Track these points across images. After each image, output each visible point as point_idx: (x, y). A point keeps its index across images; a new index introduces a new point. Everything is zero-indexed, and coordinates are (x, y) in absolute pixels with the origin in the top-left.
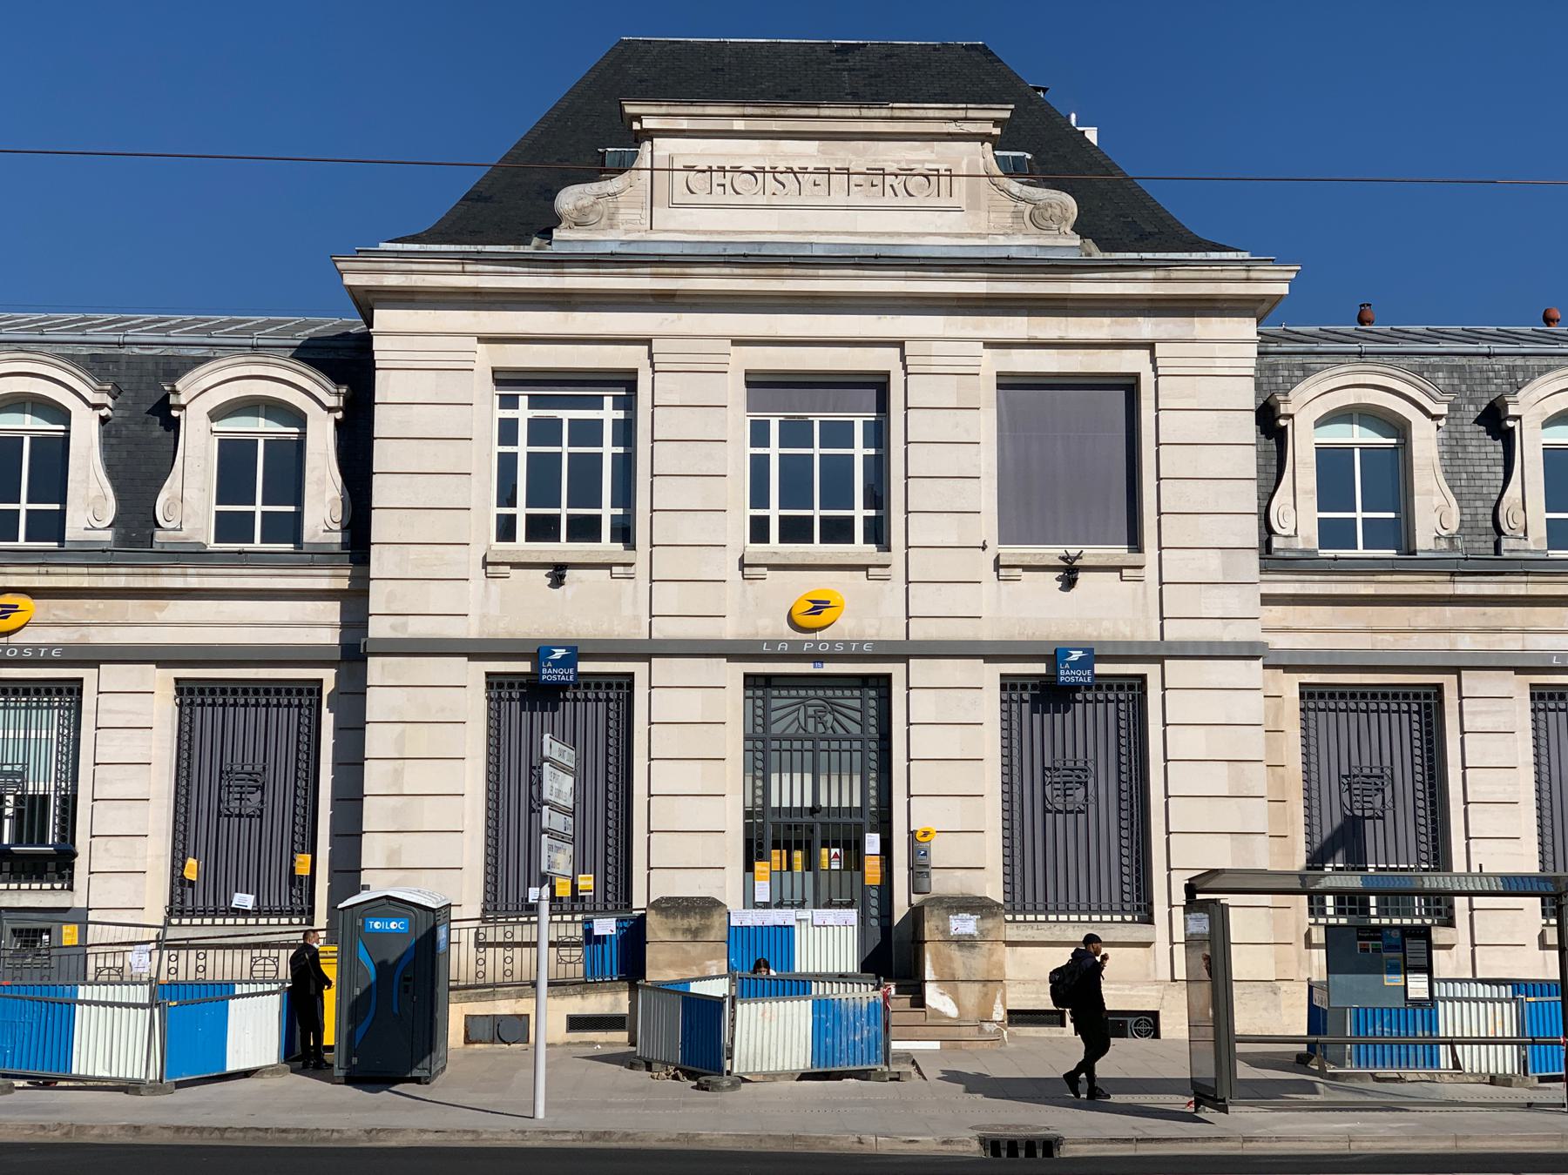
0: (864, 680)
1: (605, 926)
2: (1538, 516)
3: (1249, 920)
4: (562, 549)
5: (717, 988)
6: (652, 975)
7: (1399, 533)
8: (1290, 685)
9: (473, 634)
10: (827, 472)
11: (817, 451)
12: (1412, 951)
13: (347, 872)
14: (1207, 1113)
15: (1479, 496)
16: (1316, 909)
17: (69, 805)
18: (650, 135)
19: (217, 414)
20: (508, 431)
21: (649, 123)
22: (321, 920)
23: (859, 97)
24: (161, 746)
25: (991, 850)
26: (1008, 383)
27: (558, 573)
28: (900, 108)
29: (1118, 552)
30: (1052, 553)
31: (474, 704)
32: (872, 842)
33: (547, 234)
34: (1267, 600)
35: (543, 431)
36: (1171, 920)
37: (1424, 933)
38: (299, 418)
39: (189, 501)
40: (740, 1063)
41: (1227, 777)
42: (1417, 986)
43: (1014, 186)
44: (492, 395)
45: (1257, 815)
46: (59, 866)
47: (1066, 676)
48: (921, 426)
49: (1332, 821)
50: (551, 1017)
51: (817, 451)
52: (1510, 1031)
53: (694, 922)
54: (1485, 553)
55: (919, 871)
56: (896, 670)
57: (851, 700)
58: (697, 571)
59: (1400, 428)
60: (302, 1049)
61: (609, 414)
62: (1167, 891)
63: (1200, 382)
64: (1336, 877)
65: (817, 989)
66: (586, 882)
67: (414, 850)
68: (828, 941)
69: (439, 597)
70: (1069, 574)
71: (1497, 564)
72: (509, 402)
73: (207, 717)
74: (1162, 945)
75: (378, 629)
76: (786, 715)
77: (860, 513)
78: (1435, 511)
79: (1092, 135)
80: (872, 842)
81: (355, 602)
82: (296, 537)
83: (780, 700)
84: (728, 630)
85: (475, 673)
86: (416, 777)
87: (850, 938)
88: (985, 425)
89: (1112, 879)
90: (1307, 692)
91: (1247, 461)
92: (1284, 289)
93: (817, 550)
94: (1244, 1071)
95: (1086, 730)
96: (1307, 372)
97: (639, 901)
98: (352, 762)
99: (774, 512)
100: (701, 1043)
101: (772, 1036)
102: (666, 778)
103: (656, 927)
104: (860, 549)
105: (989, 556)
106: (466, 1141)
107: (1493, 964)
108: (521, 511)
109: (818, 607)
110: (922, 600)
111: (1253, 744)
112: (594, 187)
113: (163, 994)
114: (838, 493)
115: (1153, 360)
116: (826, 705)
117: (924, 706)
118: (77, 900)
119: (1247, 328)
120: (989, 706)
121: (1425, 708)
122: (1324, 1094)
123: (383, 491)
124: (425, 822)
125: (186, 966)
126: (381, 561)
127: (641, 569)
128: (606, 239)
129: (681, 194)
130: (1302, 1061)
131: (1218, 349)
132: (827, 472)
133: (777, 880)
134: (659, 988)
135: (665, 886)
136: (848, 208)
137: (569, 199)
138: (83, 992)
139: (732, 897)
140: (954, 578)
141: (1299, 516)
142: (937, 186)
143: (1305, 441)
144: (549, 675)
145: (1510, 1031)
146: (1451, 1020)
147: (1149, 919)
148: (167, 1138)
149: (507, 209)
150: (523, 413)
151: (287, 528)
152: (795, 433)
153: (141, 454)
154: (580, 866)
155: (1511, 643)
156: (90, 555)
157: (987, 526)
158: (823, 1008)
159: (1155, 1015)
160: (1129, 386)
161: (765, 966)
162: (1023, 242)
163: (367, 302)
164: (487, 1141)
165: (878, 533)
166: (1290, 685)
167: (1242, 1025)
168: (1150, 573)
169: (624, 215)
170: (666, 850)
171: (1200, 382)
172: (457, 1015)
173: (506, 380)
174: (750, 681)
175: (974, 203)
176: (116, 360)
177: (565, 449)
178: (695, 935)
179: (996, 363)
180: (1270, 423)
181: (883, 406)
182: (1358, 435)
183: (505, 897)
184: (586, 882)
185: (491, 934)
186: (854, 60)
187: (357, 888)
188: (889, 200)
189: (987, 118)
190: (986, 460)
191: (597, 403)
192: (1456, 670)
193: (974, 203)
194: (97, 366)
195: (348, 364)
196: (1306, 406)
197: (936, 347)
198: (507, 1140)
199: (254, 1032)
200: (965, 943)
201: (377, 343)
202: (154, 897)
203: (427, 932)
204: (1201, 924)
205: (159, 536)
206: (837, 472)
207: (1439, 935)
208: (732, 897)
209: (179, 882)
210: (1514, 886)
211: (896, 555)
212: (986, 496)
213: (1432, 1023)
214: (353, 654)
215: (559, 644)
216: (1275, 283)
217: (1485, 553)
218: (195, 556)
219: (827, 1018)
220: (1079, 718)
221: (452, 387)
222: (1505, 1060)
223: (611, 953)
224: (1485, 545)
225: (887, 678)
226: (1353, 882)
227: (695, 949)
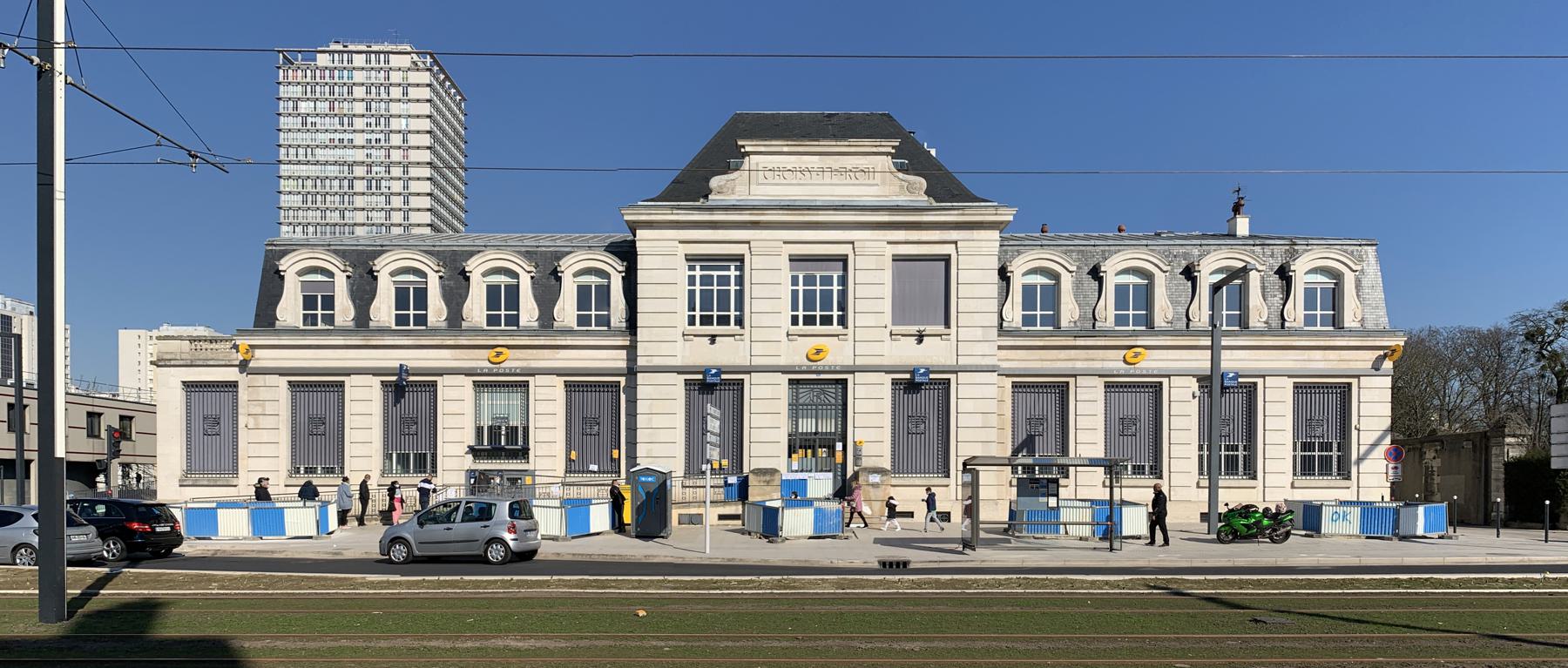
0: (837, 381)
1: (733, 480)
2: (1111, 313)
3: (986, 476)
4: (715, 329)
5: (777, 504)
6: (751, 499)
7: (1054, 321)
8: (1008, 382)
10: (822, 298)
11: (818, 288)
12: (1051, 487)
13: (632, 458)
14: (968, 551)
15: (1178, 303)
16: (1014, 471)
17: (526, 430)
18: (748, 154)
19: (576, 275)
20: (692, 280)
22: (623, 475)
23: (835, 137)
24: (560, 407)
26: (897, 259)
27: (713, 338)
28: (853, 141)
29: (941, 329)
30: (914, 329)
31: (680, 391)
32: (839, 446)
33: (706, 197)
34: (1000, 348)
35: (706, 280)
36: (956, 475)
37: (1056, 481)
39: (566, 310)
40: (784, 533)
41: (982, 420)
42: (1052, 502)
43: (900, 175)
44: (686, 265)
45: (992, 435)
46: (523, 453)
47: (918, 379)
48: (861, 277)
49: (1022, 436)
50: (711, 515)
51: (818, 288)
52: (1089, 519)
53: (768, 478)
54: (1090, 328)
55: (857, 457)
56: (849, 377)
57: (831, 389)
58: (769, 337)
59: (1056, 276)
60: (618, 526)
61: (733, 273)
62: (955, 465)
63: (976, 256)
64: (1022, 459)
65: (816, 504)
66: (725, 462)
67: (657, 450)
68: (821, 485)
69: (665, 349)
70: (920, 338)
71: (1094, 332)
72: (692, 268)
73: (576, 396)
74: (953, 486)
75: (641, 362)
76: (806, 395)
77: (835, 313)
78: (1070, 311)
79: (933, 152)
80: (839, 446)
81: (632, 350)
82: (608, 325)
83: (802, 389)
84: (782, 361)
85: (887, 379)
86: (657, 421)
87: (830, 483)
88: (887, 277)
89: (934, 463)
90: (1015, 385)
91: (993, 290)
92: (1011, 218)
93: (818, 328)
94: (982, 535)
95: (927, 399)
96: (1019, 253)
97: (746, 470)
98: (632, 415)
99: (801, 313)
100: (770, 526)
101: (797, 522)
103: (752, 480)
104: (835, 328)
106: (680, 561)
107: (1084, 493)
108: (698, 313)
109: (818, 351)
110: (963, 348)
111: (992, 406)
113: (565, 503)
114: (827, 305)
116: (821, 391)
118: (530, 467)
119: (995, 234)
121: (1061, 391)
122: (1014, 543)
123: (642, 305)
124: (661, 435)
125: (573, 493)
126: (642, 334)
127: (747, 337)
128: (731, 199)
130: (1006, 531)
132: (822, 298)
133: (801, 461)
134: (753, 504)
137: (715, 182)
138: (535, 502)
139: (783, 468)
140: (873, 340)
141: (1014, 314)
142: (867, 175)
143: (1018, 282)
144: (710, 380)
145: (1089, 519)
146: (1065, 515)
148: (570, 558)
149: (690, 187)
150: (698, 273)
151: (605, 321)
152: (809, 280)
153: (548, 290)
154: (722, 456)
155: (1097, 365)
156: (529, 332)
157: (887, 318)
158: (817, 511)
160: (946, 259)
161: (796, 495)
162: (903, 199)
163: (633, 227)
164: (687, 561)
165: (843, 321)
166: (1008, 382)
168: (953, 337)
171: (976, 256)
172: (675, 513)
173: (690, 259)
174: (791, 381)
175: (884, 183)
176: (536, 253)
177: (715, 288)
180: (1004, 274)
181: (845, 269)
182: (1039, 280)
183: (694, 466)
184: (725, 462)
185: (687, 483)
186: (834, 120)
187: (636, 465)
188: (848, 181)
189: (889, 145)
190: (887, 291)
191: (728, 268)
192: (1264, 376)
193: (884, 183)
194: (529, 255)
195: (626, 252)
196: (1018, 268)
198: (695, 561)
199: (600, 518)
200: (875, 485)
201: (638, 244)
202: (560, 466)
203: (663, 481)
204: (968, 478)
206: (827, 296)
207: (1062, 482)
208: (783, 468)
209: (569, 460)
210: (1093, 463)
212: (887, 306)
213: (1058, 517)
214: (632, 372)
216: (1007, 215)
217: (1090, 328)
218: (569, 332)
219: (820, 515)
220: (923, 395)
222: (1086, 531)
223: (735, 490)
224: (1182, 325)
226: (1030, 461)
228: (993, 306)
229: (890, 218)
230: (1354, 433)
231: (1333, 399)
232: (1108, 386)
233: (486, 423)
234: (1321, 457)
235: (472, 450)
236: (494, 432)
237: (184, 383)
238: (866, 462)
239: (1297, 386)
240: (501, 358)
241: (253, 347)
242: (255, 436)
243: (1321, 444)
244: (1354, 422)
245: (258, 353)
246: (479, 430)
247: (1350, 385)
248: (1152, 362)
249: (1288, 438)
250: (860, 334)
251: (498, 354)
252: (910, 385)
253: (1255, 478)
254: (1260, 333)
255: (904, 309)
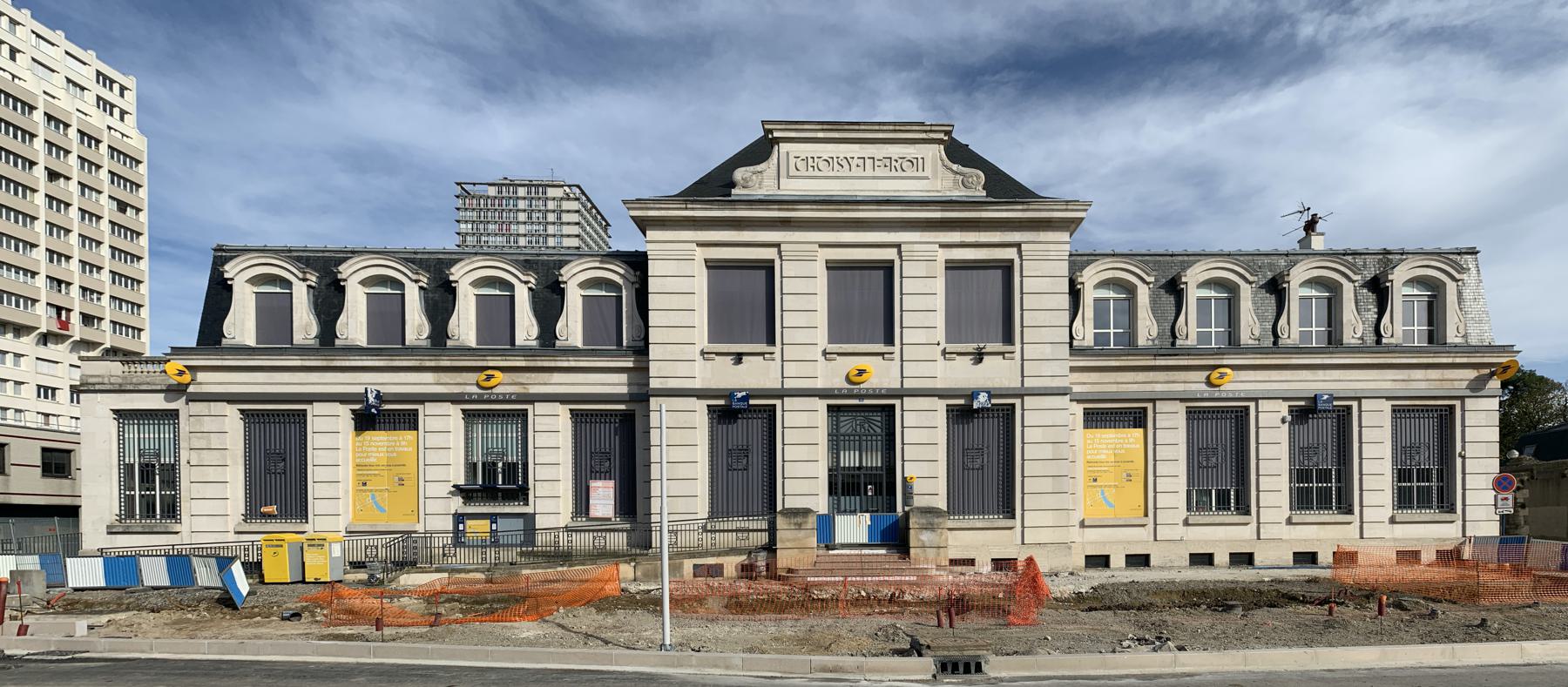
2: (1193, 330)
9: (698, 386)
17: (525, 465)
21: (776, 134)
25: (941, 486)
26: (952, 266)
29: (999, 347)
30: (971, 347)
34: (1073, 369)
38: (289, 284)
53: (799, 520)
58: (806, 354)
69: (682, 369)
81: (641, 372)
84: (820, 384)
85: (701, 406)
88: (939, 285)
91: (1064, 301)
95: (746, 432)
102: (790, 453)
105: (820, 350)
109: (861, 372)
110: (790, 369)
112: (751, 168)
115: (780, 252)
116: (866, 420)
117: (910, 419)
120: (941, 419)
129: (793, 172)
131: (1052, 247)
135: (791, 503)
136: (874, 178)
143: (1089, 295)
147: (1013, 517)
157: (940, 334)
159: (1107, 557)
162: (958, 193)
167: (103, 584)
169: (766, 182)
170: (790, 486)
178: (799, 527)
179: (944, 255)
190: (939, 302)
197: (916, 247)
205: (337, 342)
211: (777, 350)
212: (939, 320)
214: (641, 396)
215: (740, 390)
218: (573, 352)
221: (684, 268)
224: (1269, 342)
225: (893, 406)
227: (802, 534)
228: (1065, 318)
229: (941, 217)
230: (1459, 461)
231: (1227, 427)
232: (1190, 412)
233: (478, 458)
234: (1411, 488)
235: (459, 490)
236: (489, 469)
237: (115, 411)
238: (918, 502)
239: (1395, 410)
240: (493, 382)
241: (193, 369)
242: (196, 474)
243: (1319, 471)
244: (1458, 449)
245: (201, 376)
246: (471, 468)
247: (1145, 409)
248: (1236, 384)
249: (1284, 466)
250: (909, 353)
251: (489, 378)
252: (963, 413)
253: (1350, 512)
254: (1353, 350)
255: (844, 326)
